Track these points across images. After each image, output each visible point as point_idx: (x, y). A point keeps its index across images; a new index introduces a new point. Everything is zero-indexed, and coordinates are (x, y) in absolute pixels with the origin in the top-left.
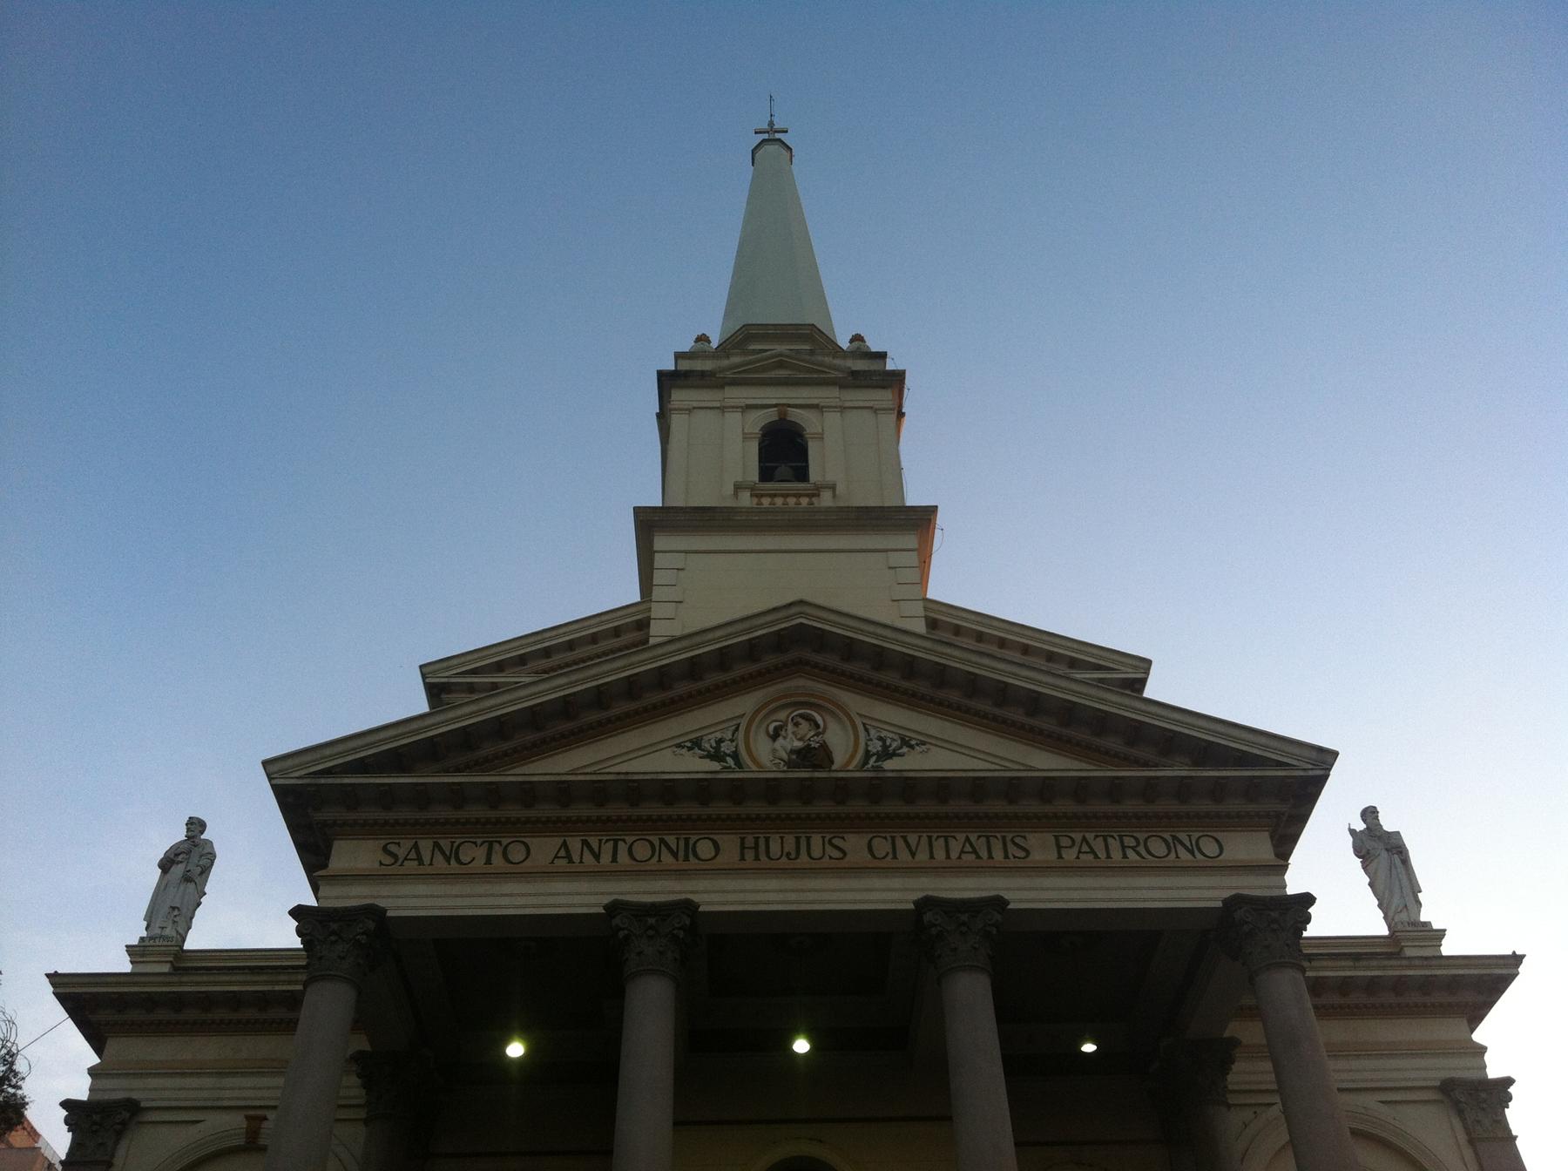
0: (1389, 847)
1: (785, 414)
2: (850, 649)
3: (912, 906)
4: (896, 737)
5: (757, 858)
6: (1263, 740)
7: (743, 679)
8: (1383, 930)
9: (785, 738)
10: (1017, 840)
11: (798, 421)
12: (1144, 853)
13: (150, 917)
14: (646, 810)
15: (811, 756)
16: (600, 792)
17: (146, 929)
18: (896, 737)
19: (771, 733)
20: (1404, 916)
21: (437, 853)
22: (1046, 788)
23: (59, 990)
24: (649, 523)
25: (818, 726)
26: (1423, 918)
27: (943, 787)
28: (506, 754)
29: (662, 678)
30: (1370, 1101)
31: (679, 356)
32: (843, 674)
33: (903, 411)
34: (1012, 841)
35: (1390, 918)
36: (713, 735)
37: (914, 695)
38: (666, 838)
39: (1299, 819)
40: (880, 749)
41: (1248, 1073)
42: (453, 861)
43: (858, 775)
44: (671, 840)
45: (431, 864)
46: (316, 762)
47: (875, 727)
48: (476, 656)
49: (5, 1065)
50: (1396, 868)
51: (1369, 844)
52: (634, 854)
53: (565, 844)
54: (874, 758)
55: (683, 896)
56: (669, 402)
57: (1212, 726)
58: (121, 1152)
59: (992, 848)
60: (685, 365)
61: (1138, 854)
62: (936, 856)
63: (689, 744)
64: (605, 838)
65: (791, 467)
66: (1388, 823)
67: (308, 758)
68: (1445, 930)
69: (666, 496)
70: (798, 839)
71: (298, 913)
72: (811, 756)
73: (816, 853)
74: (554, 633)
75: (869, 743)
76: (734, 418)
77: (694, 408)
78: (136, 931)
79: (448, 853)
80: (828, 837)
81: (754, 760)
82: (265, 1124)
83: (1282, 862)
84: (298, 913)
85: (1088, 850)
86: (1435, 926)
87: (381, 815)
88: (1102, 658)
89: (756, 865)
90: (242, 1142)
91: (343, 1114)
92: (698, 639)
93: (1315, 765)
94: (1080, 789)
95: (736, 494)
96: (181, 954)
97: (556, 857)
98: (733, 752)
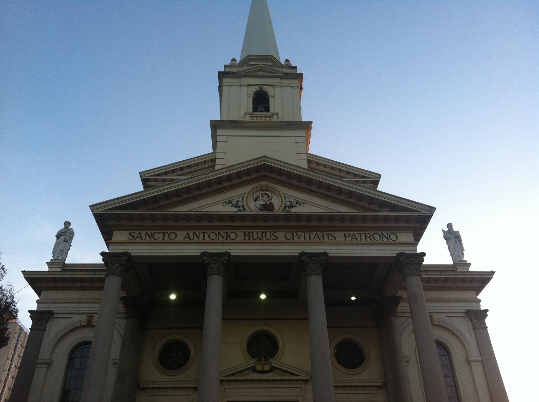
0: (455, 236)
1: (262, 88)
2: (280, 172)
3: (298, 255)
4: (295, 201)
5: (249, 239)
6: (412, 204)
7: (245, 181)
8: (451, 263)
9: (259, 201)
10: (332, 234)
11: (266, 90)
12: (372, 239)
13: (54, 253)
14: (214, 223)
15: (268, 207)
16: (199, 217)
17: (53, 257)
18: (295, 201)
19: (255, 199)
20: (458, 259)
21: (147, 236)
22: (342, 218)
23: (25, 276)
24: (215, 126)
25: (269, 197)
26: (464, 259)
27: (309, 218)
28: (168, 204)
29: (219, 181)
30: (443, 316)
31: (226, 66)
32: (278, 180)
33: (302, 87)
34: (331, 235)
35: (454, 259)
36: (236, 200)
37: (301, 187)
38: (220, 232)
39: (423, 229)
40: (289, 205)
41: (403, 307)
42: (152, 238)
43: (282, 213)
44: (222, 233)
45: (145, 239)
46: (107, 206)
47: (288, 198)
48: (158, 170)
49: (10, 299)
50: (457, 243)
51: (449, 235)
52: (210, 237)
53: (188, 234)
54: (287, 208)
55: (226, 251)
56: (222, 83)
57: (396, 199)
58: (48, 326)
59: (324, 236)
60: (228, 70)
61: (370, 239)
62: (306, 239)
63: (228, 202)
64: (201, 232)
65: (263, 107)
66: (455, 229)
67: (104, 205)
68: (471, 263)
69: (221, 111)
70: (262, 233)
71: (102, 254)
72: (268, 207)
73: (268, 237)
74: (184, 162)
75: (286, 203)
76: (244, 89)
77: (231, 85)
78: (50, 257)
79: (150, 236)
80: (272, 233)
81: (250, 209)
82: (93, 318)
83: (416, 242)
84: (102, 254)
85: (355, 238)
86: (468, 262)
87: (128, 223)
88: (365, 174)
89: (249, 241)
90: (86, 324)
91: (118, 315)
92: (231, 168)
93: (429, 212)
94: (353, 218)
95: (245, 116)
96: (64, 265)
97: (185, 237)
98: (242, 205)
